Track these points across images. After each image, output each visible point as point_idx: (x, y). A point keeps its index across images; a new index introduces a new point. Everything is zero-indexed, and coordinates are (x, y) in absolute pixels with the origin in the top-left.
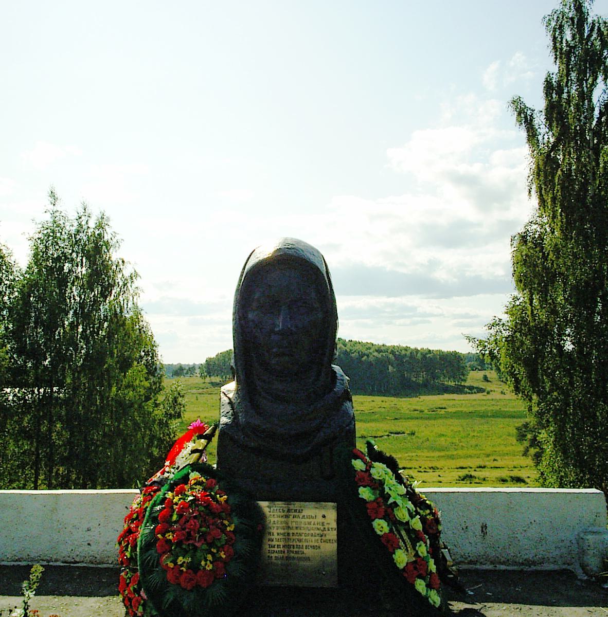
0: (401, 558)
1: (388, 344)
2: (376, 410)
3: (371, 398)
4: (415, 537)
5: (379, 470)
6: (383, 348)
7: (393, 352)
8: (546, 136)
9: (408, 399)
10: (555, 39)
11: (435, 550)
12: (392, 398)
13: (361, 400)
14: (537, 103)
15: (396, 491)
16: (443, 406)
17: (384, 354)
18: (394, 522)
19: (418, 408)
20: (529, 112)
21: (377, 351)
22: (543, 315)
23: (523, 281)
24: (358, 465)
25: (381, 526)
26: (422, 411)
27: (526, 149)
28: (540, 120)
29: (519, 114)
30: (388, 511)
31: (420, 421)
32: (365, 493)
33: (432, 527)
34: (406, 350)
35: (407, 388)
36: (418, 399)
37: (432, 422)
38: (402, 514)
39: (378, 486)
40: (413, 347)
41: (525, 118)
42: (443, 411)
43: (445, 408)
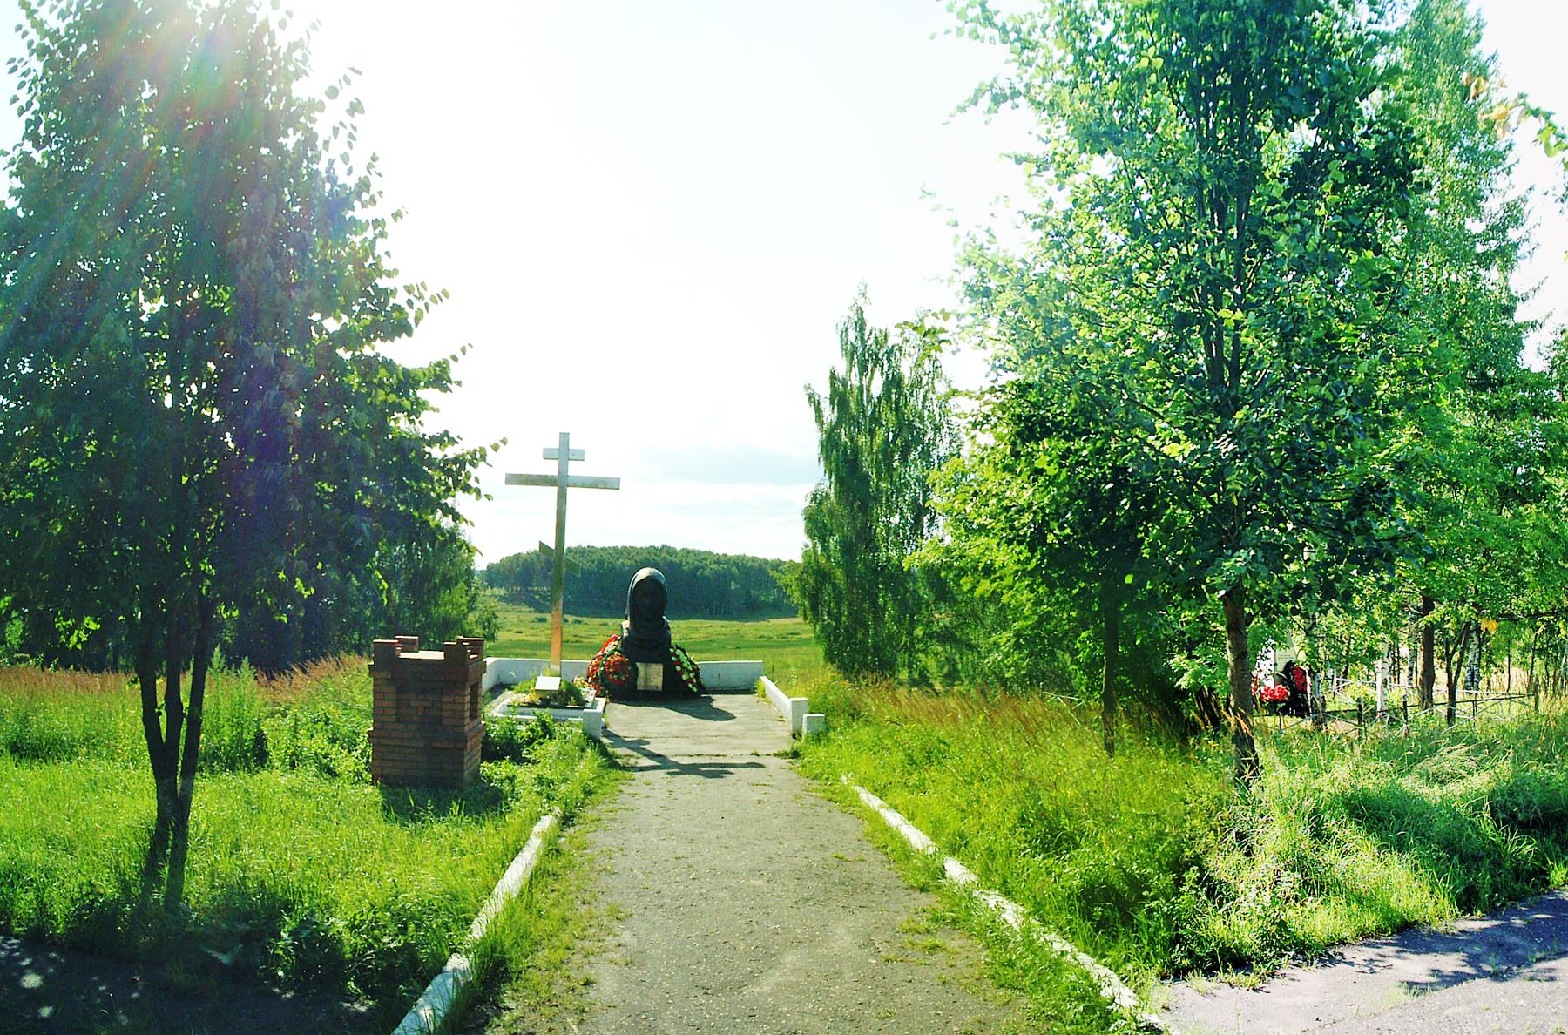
0: (684, 677)
1: (730, 554)
2: (713, 637)
3: (709, 623)
4: (689, 672)
5: (678, 652)
6: (723, 559)
7: (736, 564)
8: (830, 415)
9: (754, 623)
10: (842, 340)
11: (697, 676)
12: (735, 623)
13: (695, 626)
14: (824, 391)
15: (683, 658)
16: (797, 631)
17: (725, 566)
18: (683, 668)
19: (766, 634)
20: (817, 398)
21: (715, 563)
22: (823, 561)
23: (810, 533)
24: (672, 650)
25: (678, 668)
26: (770, 638)
27: (815, 426)
28: (825, 405)
29: (810, 398)
30: (681, 664)
31: (765, 651)
32: (673, 659)
33: (696, 671)
34: (753, 561)
35: (751, 609)
36: (766, 623)
37: (781, 650)
38: (685, 665)
39: (678, 656)
40: (761, 557)
41: (814, 401)
42: (795, 638)
43: (798, 634)
